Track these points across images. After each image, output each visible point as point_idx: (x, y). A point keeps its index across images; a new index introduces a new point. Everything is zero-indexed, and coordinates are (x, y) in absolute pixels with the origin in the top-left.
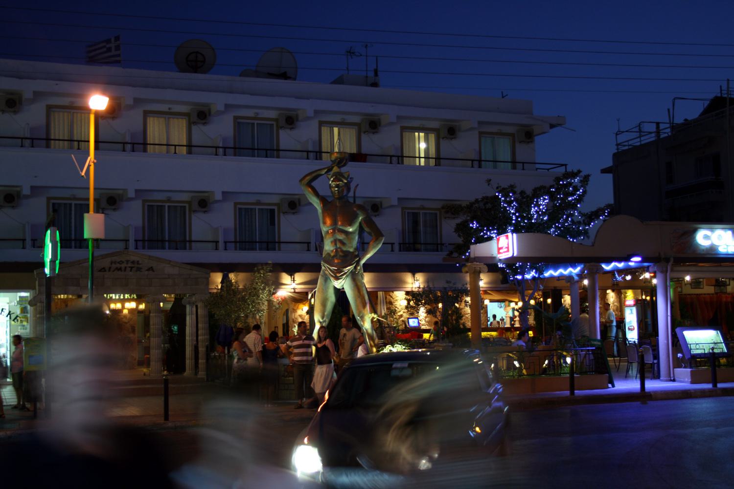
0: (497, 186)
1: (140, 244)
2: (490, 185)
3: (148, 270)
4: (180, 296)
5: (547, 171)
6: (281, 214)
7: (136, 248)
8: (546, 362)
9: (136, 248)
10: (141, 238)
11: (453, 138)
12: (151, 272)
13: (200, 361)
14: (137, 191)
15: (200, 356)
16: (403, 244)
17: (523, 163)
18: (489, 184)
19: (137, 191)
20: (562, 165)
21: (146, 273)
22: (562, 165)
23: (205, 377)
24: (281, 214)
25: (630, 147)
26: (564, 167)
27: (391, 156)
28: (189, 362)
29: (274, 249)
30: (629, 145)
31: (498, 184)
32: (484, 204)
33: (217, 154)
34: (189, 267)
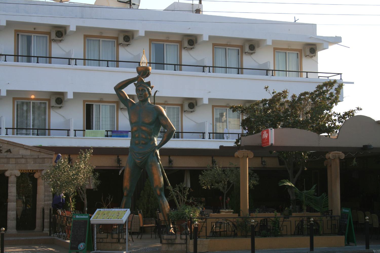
0: (273, 91)
1: (10, 131)
2: (267, 90)
3: (7, 152)
4: (33, 171)
5: (327, 78)
6: (119, 110)
7: (210, 138)
8: (26, 223)
9: (210, 138)
10: (212, 132)
11: (253, 53)
12: (9, 153)
13: (45, 220)
14: (8, 91)
15: (45, 216)
16: (213, 133)
17: (307, 72)
18: (266, 90)
19: (8, 91)
20: (339, 74)
21: (5, 154)
22: (339, 74)
23: (49, 232)
24: (119, 110)
25: (71, 54)
26: (340, 75)
27: (209, 67)
28: (38, 221)
29: (45, 134)
30: (72, 53)
31: (274, 90)
32: (263, 105)
33: (70, 64)
34: (35, 148)
